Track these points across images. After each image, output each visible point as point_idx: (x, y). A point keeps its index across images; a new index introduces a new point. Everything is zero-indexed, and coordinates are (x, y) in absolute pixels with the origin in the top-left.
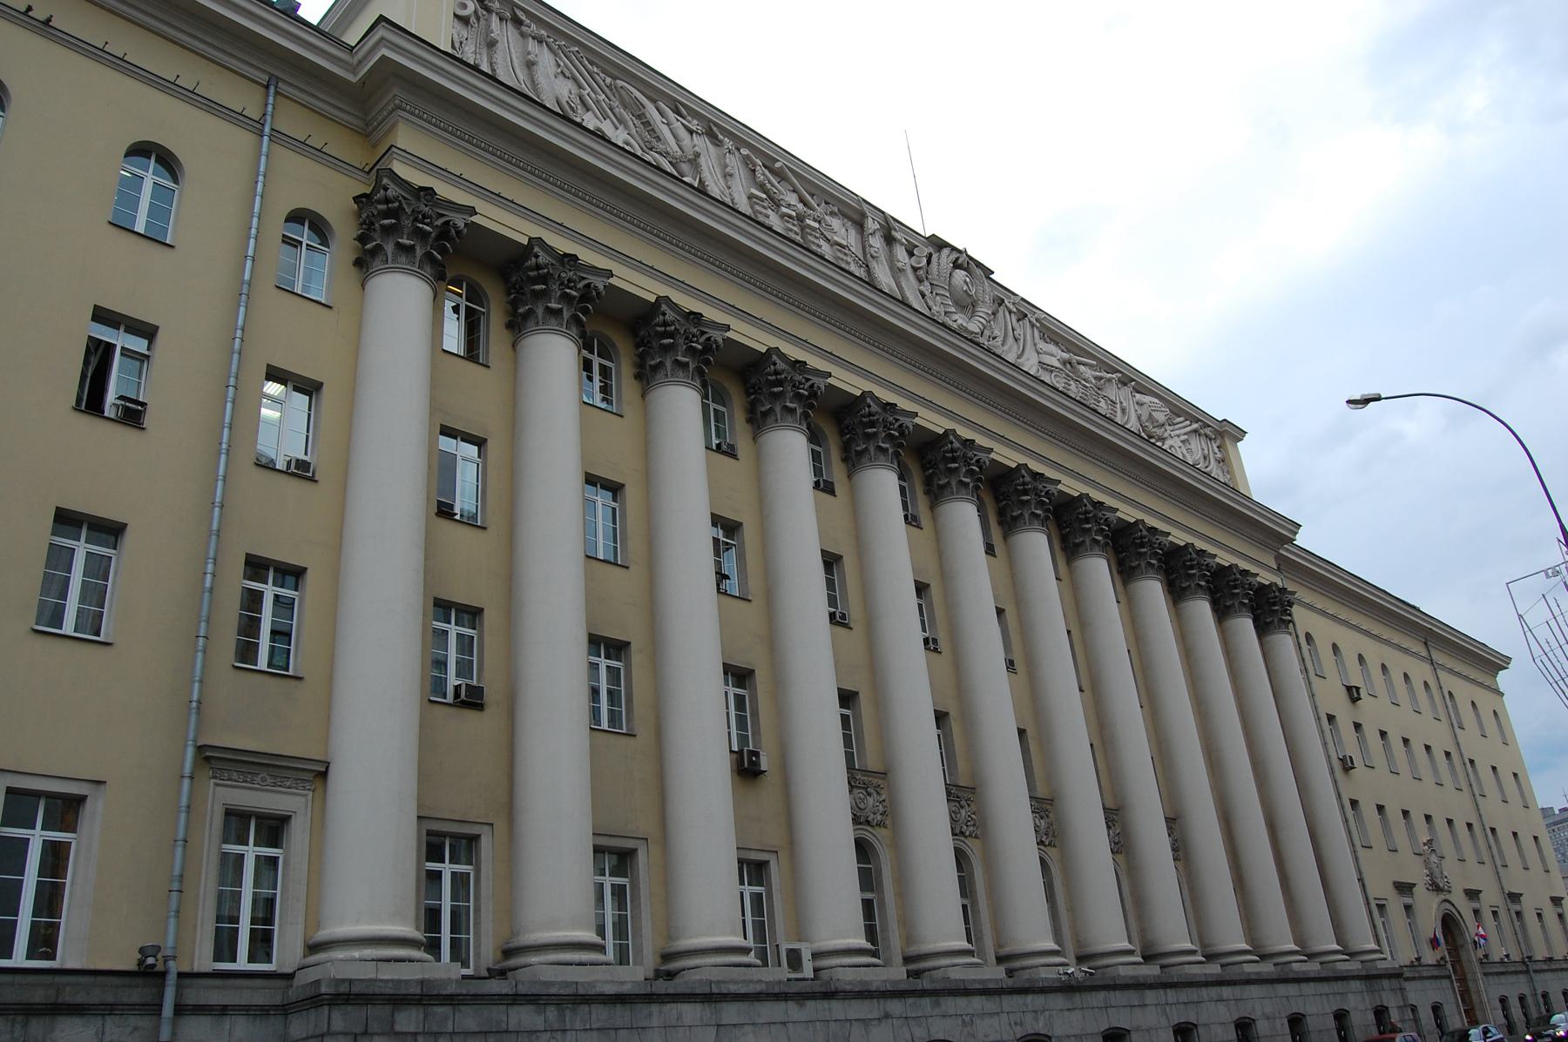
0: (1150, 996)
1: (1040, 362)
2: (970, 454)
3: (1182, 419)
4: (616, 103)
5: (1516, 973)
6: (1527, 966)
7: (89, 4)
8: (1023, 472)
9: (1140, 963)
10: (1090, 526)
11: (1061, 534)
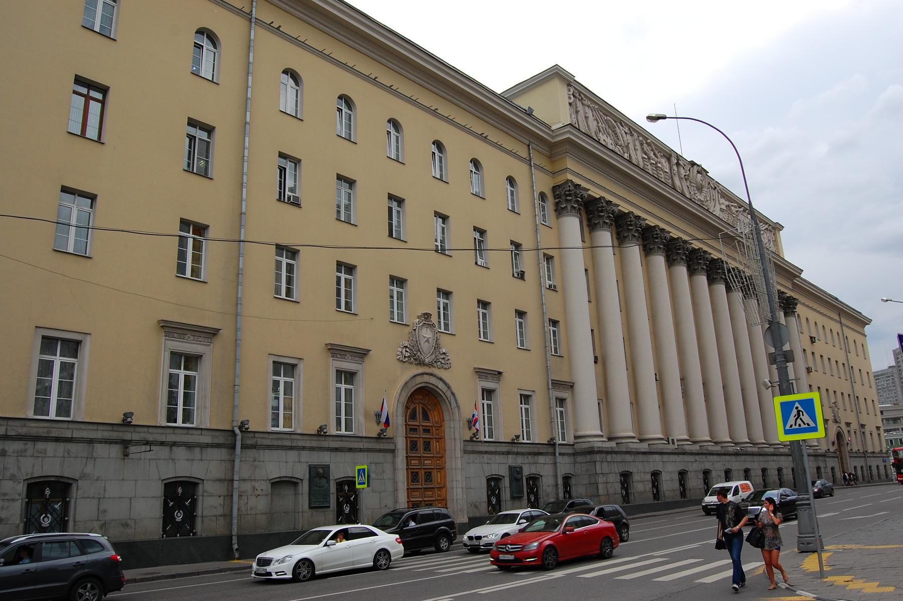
0: (756, 458)
1: (721, 208)
2: (578, 192)
3: (762, 224)
4: (607, 127)
5: (861, 457)
6: (865, 455)
7: (266, 2)
8: (602, 201)
9: (605, 442)
10: (632, 227)
11: (588, 218)
